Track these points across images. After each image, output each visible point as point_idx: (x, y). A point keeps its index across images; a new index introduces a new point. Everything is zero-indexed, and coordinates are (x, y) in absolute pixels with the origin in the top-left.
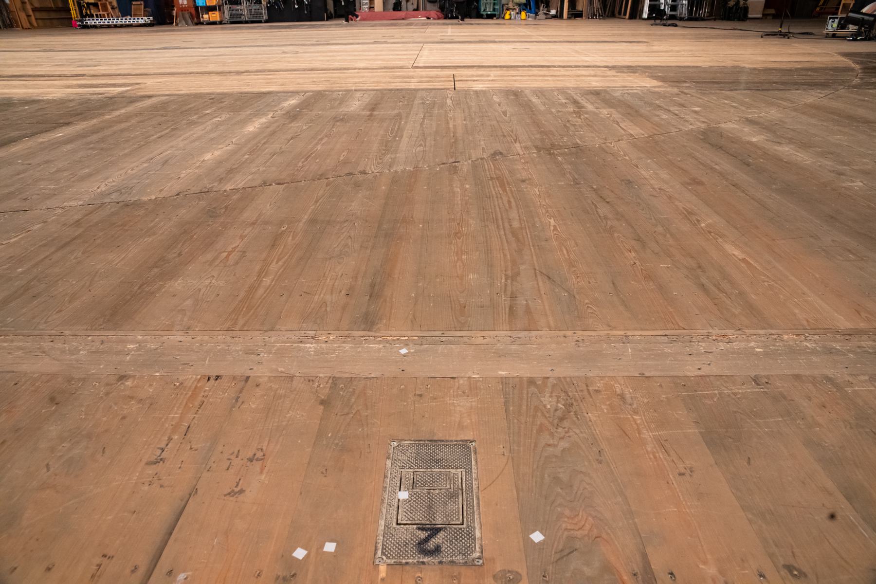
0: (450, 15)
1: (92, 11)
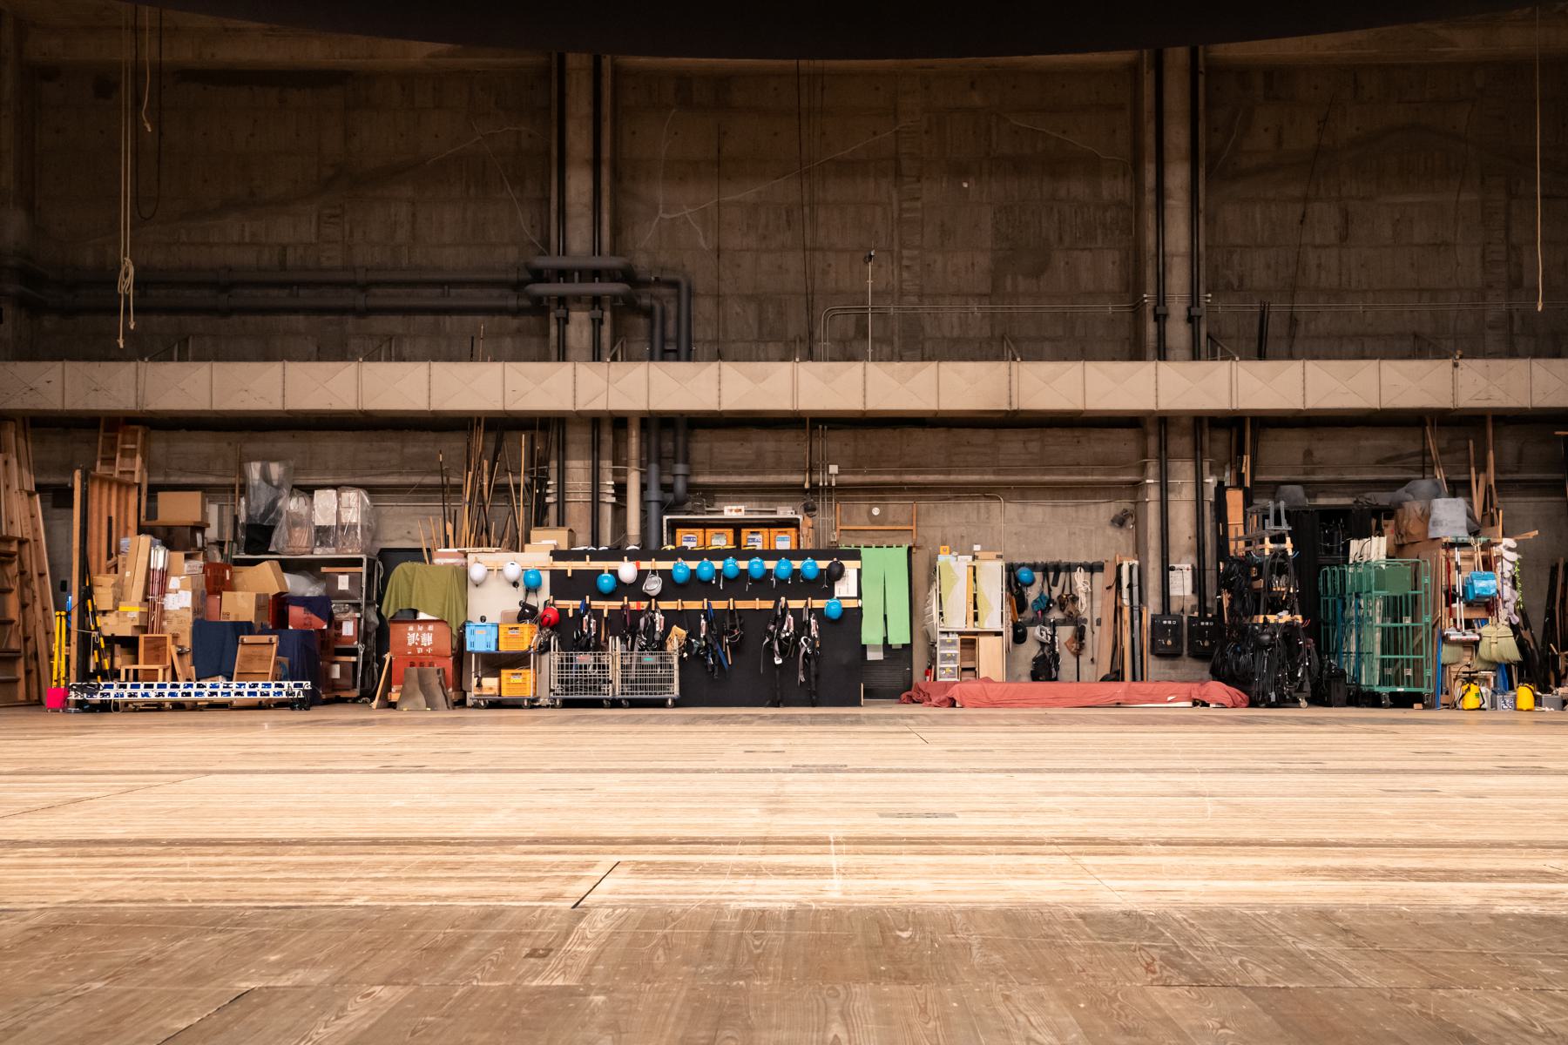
0: (1273, 696)
1: (118, 662)
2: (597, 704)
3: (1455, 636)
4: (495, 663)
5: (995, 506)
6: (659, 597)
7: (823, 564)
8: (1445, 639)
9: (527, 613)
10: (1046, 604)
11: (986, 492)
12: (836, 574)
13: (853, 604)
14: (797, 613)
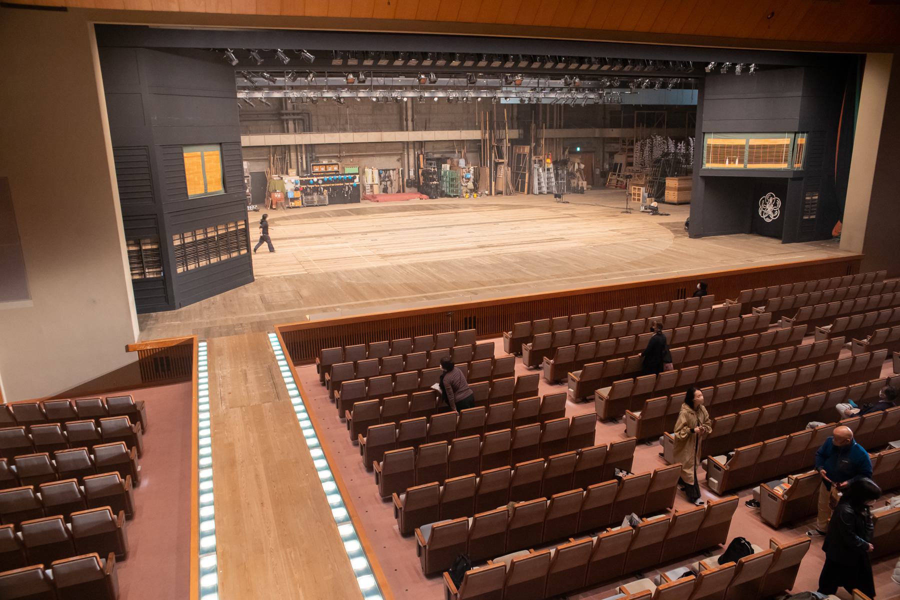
2: (313, 206)
3: (464, 185)
4: (293, 200)
5: (374, 158)
6: (322, 184)
7: (352, 176)
8: (462, 185)
9: (296, 189)
10: (385, 177)
11: (373, 155)
12: (354, 178)
13: (358, 183)
14: (348, 186)
